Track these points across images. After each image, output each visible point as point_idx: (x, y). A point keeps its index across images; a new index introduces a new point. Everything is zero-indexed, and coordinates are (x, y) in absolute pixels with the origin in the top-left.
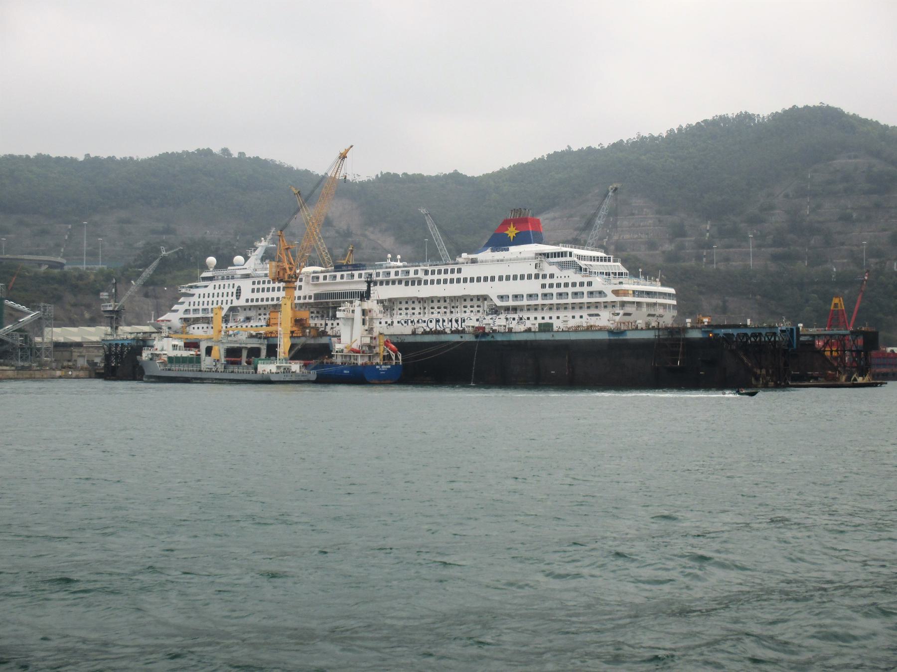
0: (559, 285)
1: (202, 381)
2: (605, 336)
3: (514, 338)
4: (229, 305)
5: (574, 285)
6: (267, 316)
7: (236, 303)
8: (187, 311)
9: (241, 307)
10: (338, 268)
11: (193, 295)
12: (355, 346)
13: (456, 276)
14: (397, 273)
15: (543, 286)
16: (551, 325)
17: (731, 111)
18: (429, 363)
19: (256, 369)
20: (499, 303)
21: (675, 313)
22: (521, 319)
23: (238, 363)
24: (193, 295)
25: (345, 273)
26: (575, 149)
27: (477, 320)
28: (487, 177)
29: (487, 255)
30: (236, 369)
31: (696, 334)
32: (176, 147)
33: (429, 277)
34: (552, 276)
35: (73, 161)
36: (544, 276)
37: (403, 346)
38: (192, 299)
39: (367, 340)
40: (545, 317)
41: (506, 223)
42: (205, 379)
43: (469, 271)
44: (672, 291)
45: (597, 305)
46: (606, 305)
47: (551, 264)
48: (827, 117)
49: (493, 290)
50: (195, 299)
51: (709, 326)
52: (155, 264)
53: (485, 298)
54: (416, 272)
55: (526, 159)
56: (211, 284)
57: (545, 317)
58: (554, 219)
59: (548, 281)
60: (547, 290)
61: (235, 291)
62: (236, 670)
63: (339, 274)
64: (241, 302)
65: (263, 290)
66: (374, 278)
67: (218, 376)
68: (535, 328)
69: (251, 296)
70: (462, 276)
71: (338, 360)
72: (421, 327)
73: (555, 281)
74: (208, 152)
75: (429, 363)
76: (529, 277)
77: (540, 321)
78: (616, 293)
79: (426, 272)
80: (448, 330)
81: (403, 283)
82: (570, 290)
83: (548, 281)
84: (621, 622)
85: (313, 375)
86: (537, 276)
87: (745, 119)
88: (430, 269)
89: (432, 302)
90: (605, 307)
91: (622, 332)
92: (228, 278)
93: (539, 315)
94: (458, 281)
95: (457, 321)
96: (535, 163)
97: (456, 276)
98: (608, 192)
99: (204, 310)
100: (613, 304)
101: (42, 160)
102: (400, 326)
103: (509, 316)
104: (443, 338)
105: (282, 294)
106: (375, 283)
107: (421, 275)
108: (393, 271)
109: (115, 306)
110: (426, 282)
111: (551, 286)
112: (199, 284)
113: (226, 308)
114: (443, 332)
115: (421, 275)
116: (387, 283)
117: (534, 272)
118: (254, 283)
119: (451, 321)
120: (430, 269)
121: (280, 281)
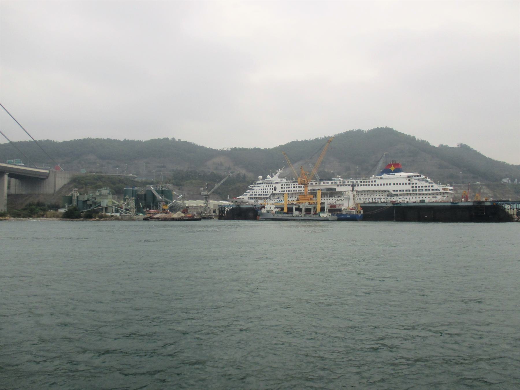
0: (419, 187)
2: (450, 204)
3: (409, 205)
5: (426, 187)
7: (274, 192)
10: (321, 180)
12: (351, 208)
13: (374, 183)
14: (340, 182)
15: (412, 187)
17: (355, 129)
18: (373, 213)
20: (393, 193)
23: (310, 214)
26: (299, 140)
28: (273, 149)
29: (385, 176)
30: (310, 215)
31: (488, 204)
32: (94, 136)
33: (362, 184)
34: (416, 184)
35: (119, 141)
36: (413, 184)
37: (363, 208)
38: (253, 191)
39: (355, 206)
40: (423, 198)
41: (390, 165)
43: (379, 182)
44: (452, 188)
46: (440, 194)
47: (415, 179)
49: (391, 188)
50: (255, 191)
54: (357, 182)
55: (284, 144)
56: (262, 186)
59: (414, 185)
60: (414, 188)
61: (273, 188)
63: (322, 182)
64: (277, 192)
65: (294, 187)
66: (355, 183)
67: (301, 218)
68: (418, 201)
69: (281, 190)
70: (376, 183)
71: (344, 213)
72: (367, 201)
73: (417, 185)
74: (167, 139)
75: (373, 213)
76: (406, 184)
77: (421, 199)
78: (444, 189)
79: (361, 182)
80: (380, 202)
82: (424, 188)
83: (414, 185)
84: (365, 287)
86: (409, 184)
87: (359, 131)
88: (362, 181)
93: (421, 197)
94: (375, 185)
96: (287, 144)
99: (255, 195)
101: (109, 141)
102: (363, 200)
104: (378, 205)
105: (303, 189)
106: (355, 186)
107: (359, 183)
108: (338, 182)
110: (361, 185)
111: (416, 187)
113: (270, 194)
114: (378, 203)
115: (359, 183)
116: (343, 185)
117: (408, 182)
120: (362, 181)
121: (302, 184)
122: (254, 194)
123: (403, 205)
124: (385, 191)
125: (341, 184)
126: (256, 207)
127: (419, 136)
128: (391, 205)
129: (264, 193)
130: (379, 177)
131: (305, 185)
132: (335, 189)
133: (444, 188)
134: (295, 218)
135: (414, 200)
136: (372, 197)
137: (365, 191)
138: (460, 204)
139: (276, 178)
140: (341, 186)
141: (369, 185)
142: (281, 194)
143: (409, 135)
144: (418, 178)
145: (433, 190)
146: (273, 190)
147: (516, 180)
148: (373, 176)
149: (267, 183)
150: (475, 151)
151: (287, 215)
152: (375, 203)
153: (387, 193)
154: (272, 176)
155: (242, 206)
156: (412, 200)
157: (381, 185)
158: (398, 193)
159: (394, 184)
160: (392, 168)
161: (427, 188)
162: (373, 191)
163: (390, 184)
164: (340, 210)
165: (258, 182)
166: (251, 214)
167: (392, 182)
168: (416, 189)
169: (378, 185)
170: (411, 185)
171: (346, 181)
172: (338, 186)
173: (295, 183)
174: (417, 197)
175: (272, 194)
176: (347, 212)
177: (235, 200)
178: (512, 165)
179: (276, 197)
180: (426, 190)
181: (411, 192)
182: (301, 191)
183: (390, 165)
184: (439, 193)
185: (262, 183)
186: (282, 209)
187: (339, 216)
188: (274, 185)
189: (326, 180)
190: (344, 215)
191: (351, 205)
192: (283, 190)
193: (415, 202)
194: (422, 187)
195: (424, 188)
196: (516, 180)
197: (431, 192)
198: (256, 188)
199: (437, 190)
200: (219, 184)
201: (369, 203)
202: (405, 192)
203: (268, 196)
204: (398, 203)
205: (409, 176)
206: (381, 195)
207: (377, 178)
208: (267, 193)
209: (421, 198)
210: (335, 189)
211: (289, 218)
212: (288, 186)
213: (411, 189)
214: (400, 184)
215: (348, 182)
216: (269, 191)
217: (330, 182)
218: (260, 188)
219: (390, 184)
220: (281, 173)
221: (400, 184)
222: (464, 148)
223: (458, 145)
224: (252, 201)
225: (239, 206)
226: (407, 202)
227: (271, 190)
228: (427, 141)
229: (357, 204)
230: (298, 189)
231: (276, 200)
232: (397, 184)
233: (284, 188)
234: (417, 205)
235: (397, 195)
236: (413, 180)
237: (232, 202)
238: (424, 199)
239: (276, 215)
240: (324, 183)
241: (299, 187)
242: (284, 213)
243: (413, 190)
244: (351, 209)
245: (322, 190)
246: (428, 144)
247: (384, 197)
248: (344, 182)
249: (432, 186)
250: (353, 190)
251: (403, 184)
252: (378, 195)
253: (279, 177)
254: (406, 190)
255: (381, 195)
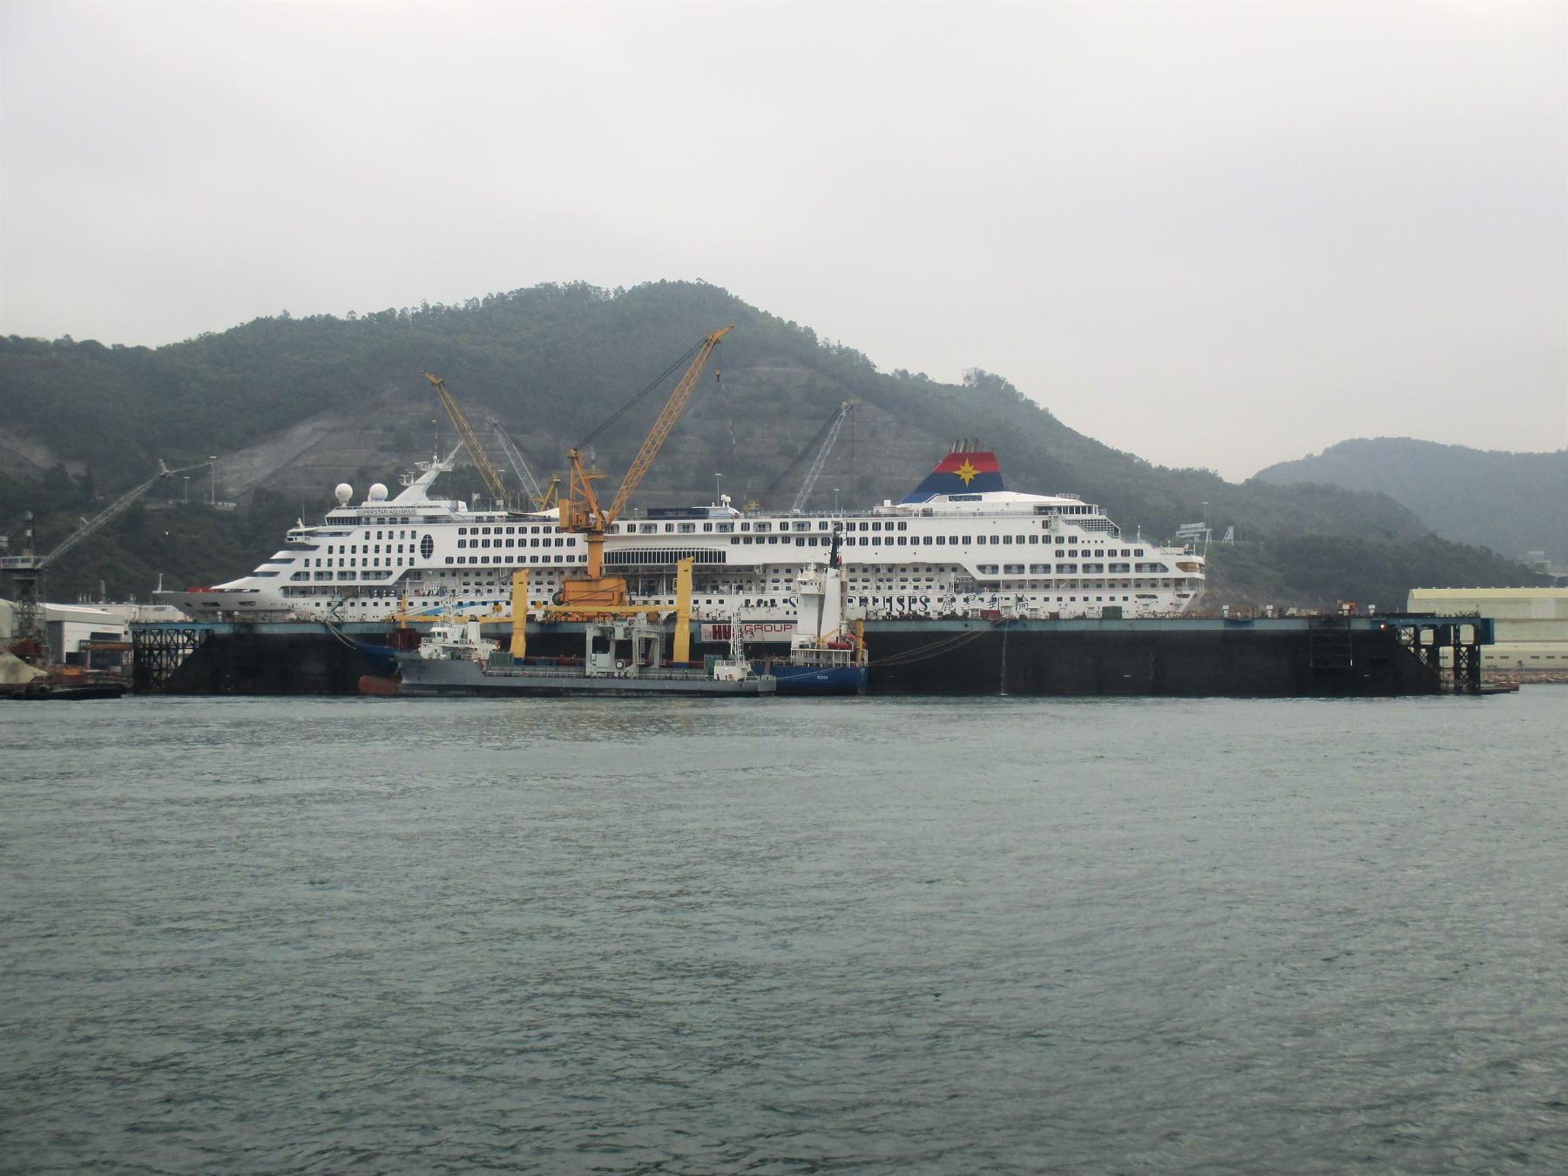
0: (1086, 553)
1: (593, 693)
2: (1218, 626)
3: (1062, 627)
4: (406, 566)
5: (1112, 553)
6: (556, 589)
7: (421, 563)
8: (297, 575)
9: (434, 570)
10: (656, 513)
11: (314, 548)
12: (832, 639)
13: (896, 534)
15: (1059, 554)
16: (1119, 610)
18: (916, 663)
19: (711, 673)
20: (979, 576)
21: (1202, 591)
22: (1020, 600)
24: (314, 548)
25: (675, 523)
26: (297, 315)
27: (940, 600)
29: (939, 503)
31: (1361, 625)
34: (1073, 540)
36: (1060, 540)
38: (312, 556)
40: (1116, 598)
42: (602, 690)
45: (1153, 584)
47: (1069, 522)
48: (702, 302)
49: (970, 558)
50: (322, 553)
51: (1376, 615)
52: (148, 485)
53: (955, 568)
56: (358, 533)
57: (1116, 598)
58: (333, 431)
59: (1066, 547)
60: (1066, 560)
61: (418, 543)
62: (504, 1171)
63: (661, 524)
64: (437, 561)
69: (457, 553)
70: (908, 534)
71: (798, 659)
73: (1079, 547)
75: (916, 663)
76: (1034, 539)
77: (1106, 603)
78: (1184, 566)
80: (934, 615)
81: (793, 541)
82: (1106, 560)
83: (1066, 547)
85: (767, 680)
86: (1047, 539)
87: (579, 294)
89: (776, 571)
90: (1166, 585)
91: (1248, 622)
92: (393, 521)
93: (1106, 594)
94: (902, 541)
95: (901, 601)
97: (896, 534)
98: (839, 410)
100: (1179, 582)
103: (997, 596)
109: (37, 562)
111: (1073, 553)
112: (320, 529)
113: (398, 572)
114: (927, 618)
116: (760, 540)
118: (462, 531)
119: (890, 600)
122: (312, 569)
123: (1035, 628)
124: (941, 568)
125: (751, 532)
126: (345, 630)
127: (832, 331)
128: (984, 627)
129: (370, 567)
130: (917, 507)
131: (594, 534)
132: (722, 556)
133: (1185, 559)
134: (596, 684)
135: (1079, 608)
136: (888, 594)
137: (916, 567)
138: (1259, 626)
139: (414, 495)
140: (748, 540)
141: (876, 541)
142: (454, 572)
143: (792, 324)
144: (1081, 516)
145: (1139, 567)
146: (418, 554)
147: (1231, 530)
148: (888, 503)
149: (381, 521)
150: (1030, 404)
151: (529, 670)
152: (915, 617)
153: (952, 577)
154: (395, 490)
155: (265, 630)
156: (1077, 606)
157: (928, 541)
158: (1001, 576)
159: (981, 540)
160: (967, 472)
161: (1119, 559)
162: (891, 568)
163: (967, 540)
164: (784, 648)
165: (334, 513)
166: (314, 667)
167: (974, 529)
168: (1098, 560)
169: (915, 541)
170: (1054, 546)
171: (776, 524)
172: (735, 540)
173: (516, 526)
174: (1092, 594)
175: (407, 574)
176: (814, 659)
177: (200, 596)
178: (1162, 469)
179: (432, 585)
180: (1113, 567)
181: (1053, 575)
182: (558, 559)
183: (956, 459)
184: (1160, 586)
185: (355, 521)
186: (505, 641)
187: (787, 675)
188: (423, 531)
189: (676, 513)
190: (804, 668)
191: (832, 628)
192: (468, 552)
193: (1083, 617)
194: (1099, 553)
195: (1106, 560)
196: (1231, 530)
197: (1133, 574)
198: (324, 542)
199: (1153, 567)
200: (101, 520)
201: (890, 618)
202: (1027, 575)
203: (390, 581)
204: (1013, 621)
205: (1041, 510)
206: (923, 584)
207: (910, 513)
208: (382, 567)
209: (1107, 599)
210: (722, 556)
211: (564, 683)
212: (492, 537)
213: (1054, 562)
214: (1007, 540)
215: (784, 526)
216: (394, 555)
217: (699, 524)
218: (347, 542)
219: (967, 540)
220: (442, 476)
221: (1007, 540)
222: (989, 388)
223: (968, 378)
224: (316, 608)
225: (250, 626)
226: (1054, 617)
227: (406, 555)
228: (862, 351)
229: (852, 625)
230: (553, 551)
231: (431, 600)
232: (995, 540)
233: (474, 544)
234: (1095, 627)
235: (994, 586)
236: (1062, 524)
237: (186, 607)
238: (1118, 603)
239: (496, 670)
240: (669, 528)
241: (559, 543)
242: (518, 662)
243: (1060, 568)
244: (831, 646)
245: (700, 556)
246: (868, 367)
247: (934, 595)
248: (762, 526)
249: (1139, 553)
250: (835, 562)
251: (1021, 540)
252: (910, 585)
253: (433, 492)
254: (1034, 568)
255: (923, 584)
